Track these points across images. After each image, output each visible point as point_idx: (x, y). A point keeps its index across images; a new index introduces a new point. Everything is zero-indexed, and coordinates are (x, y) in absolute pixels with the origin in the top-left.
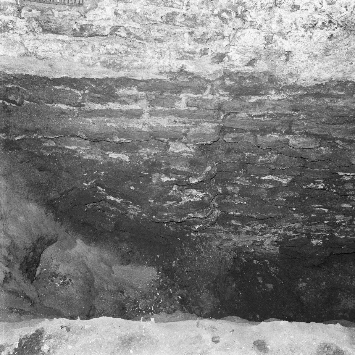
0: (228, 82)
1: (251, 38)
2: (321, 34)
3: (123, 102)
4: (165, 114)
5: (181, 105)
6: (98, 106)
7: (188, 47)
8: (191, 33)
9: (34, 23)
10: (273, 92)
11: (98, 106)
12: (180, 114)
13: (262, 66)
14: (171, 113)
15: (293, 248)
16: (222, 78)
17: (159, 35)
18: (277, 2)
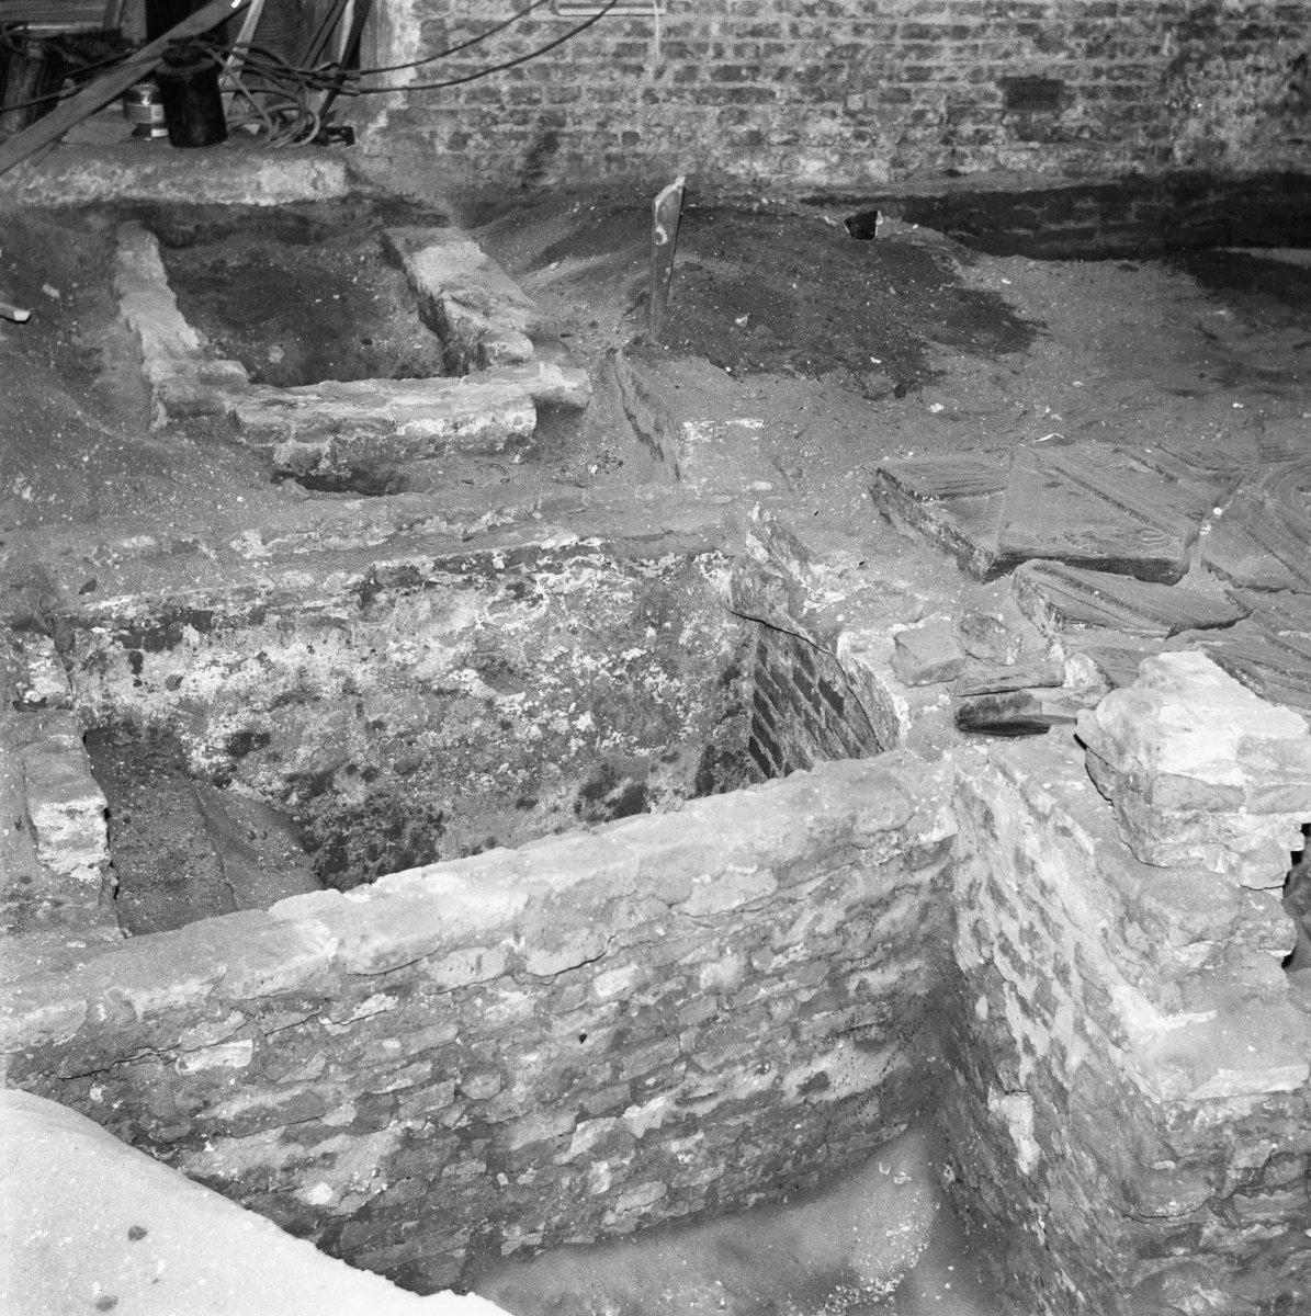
0: (1172, 185)
1: (1194, 127)
2: (1250, 119)
3: (1079, 219)
4: (1115, 229)
5: (1132, 218)
6: (1054, 227)
7: (1141, 143)
8: (1145, 128)
9: (1013, 131)
10: (1211, 193)
11: (1054, 227)
12: (1129, 228)
13: (1200, 165)
14: (1122, 228)
15: (1266, 597)
16: (1166, 181)
17: (1118, 132)
18: (886, 1226)
